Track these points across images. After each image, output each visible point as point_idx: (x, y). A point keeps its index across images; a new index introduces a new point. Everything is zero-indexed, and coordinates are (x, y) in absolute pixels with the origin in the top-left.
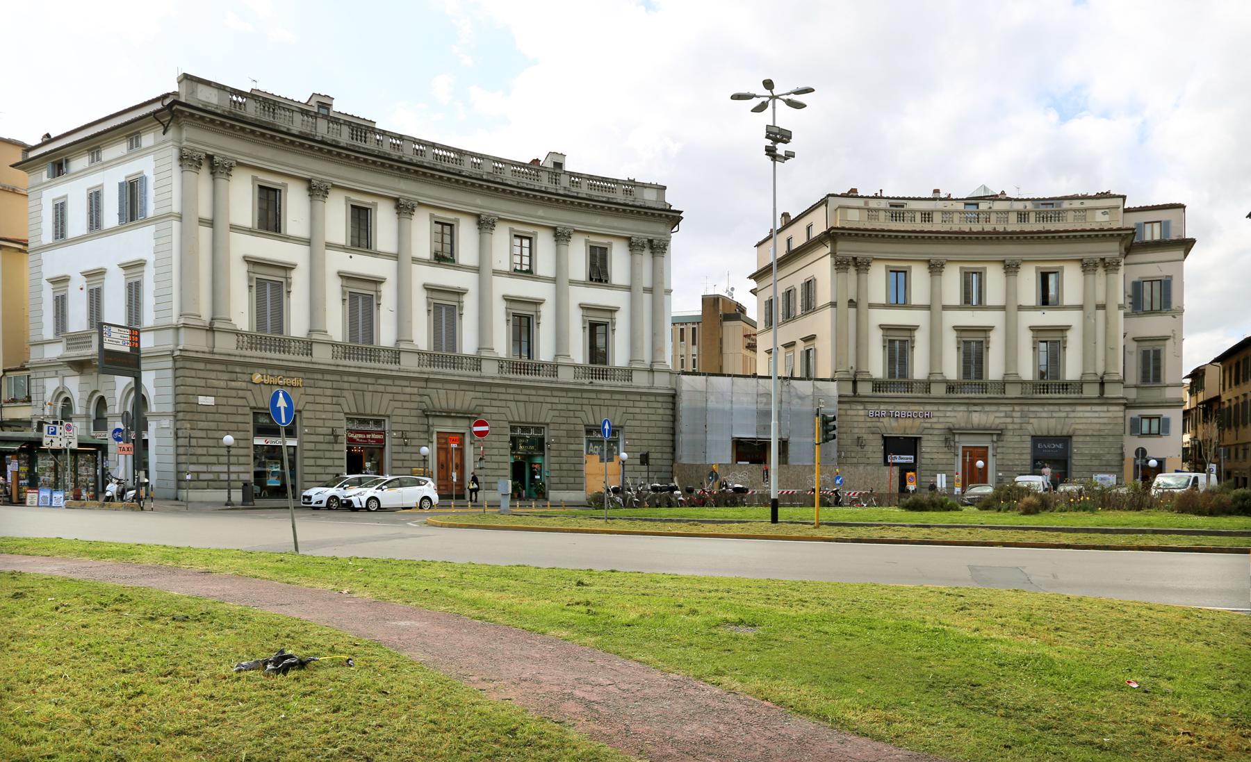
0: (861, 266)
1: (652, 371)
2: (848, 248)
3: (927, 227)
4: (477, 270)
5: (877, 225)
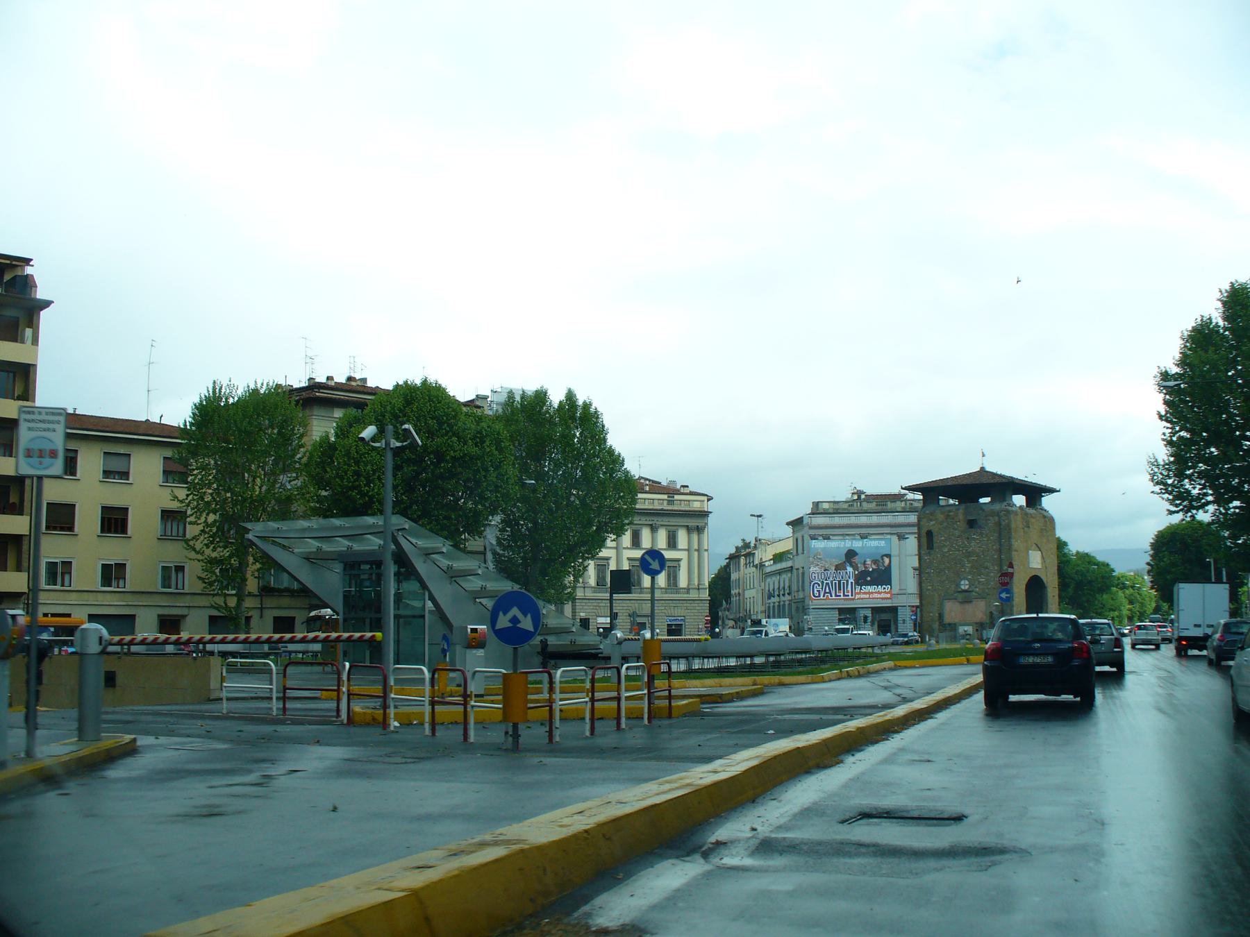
3: (670, 508)
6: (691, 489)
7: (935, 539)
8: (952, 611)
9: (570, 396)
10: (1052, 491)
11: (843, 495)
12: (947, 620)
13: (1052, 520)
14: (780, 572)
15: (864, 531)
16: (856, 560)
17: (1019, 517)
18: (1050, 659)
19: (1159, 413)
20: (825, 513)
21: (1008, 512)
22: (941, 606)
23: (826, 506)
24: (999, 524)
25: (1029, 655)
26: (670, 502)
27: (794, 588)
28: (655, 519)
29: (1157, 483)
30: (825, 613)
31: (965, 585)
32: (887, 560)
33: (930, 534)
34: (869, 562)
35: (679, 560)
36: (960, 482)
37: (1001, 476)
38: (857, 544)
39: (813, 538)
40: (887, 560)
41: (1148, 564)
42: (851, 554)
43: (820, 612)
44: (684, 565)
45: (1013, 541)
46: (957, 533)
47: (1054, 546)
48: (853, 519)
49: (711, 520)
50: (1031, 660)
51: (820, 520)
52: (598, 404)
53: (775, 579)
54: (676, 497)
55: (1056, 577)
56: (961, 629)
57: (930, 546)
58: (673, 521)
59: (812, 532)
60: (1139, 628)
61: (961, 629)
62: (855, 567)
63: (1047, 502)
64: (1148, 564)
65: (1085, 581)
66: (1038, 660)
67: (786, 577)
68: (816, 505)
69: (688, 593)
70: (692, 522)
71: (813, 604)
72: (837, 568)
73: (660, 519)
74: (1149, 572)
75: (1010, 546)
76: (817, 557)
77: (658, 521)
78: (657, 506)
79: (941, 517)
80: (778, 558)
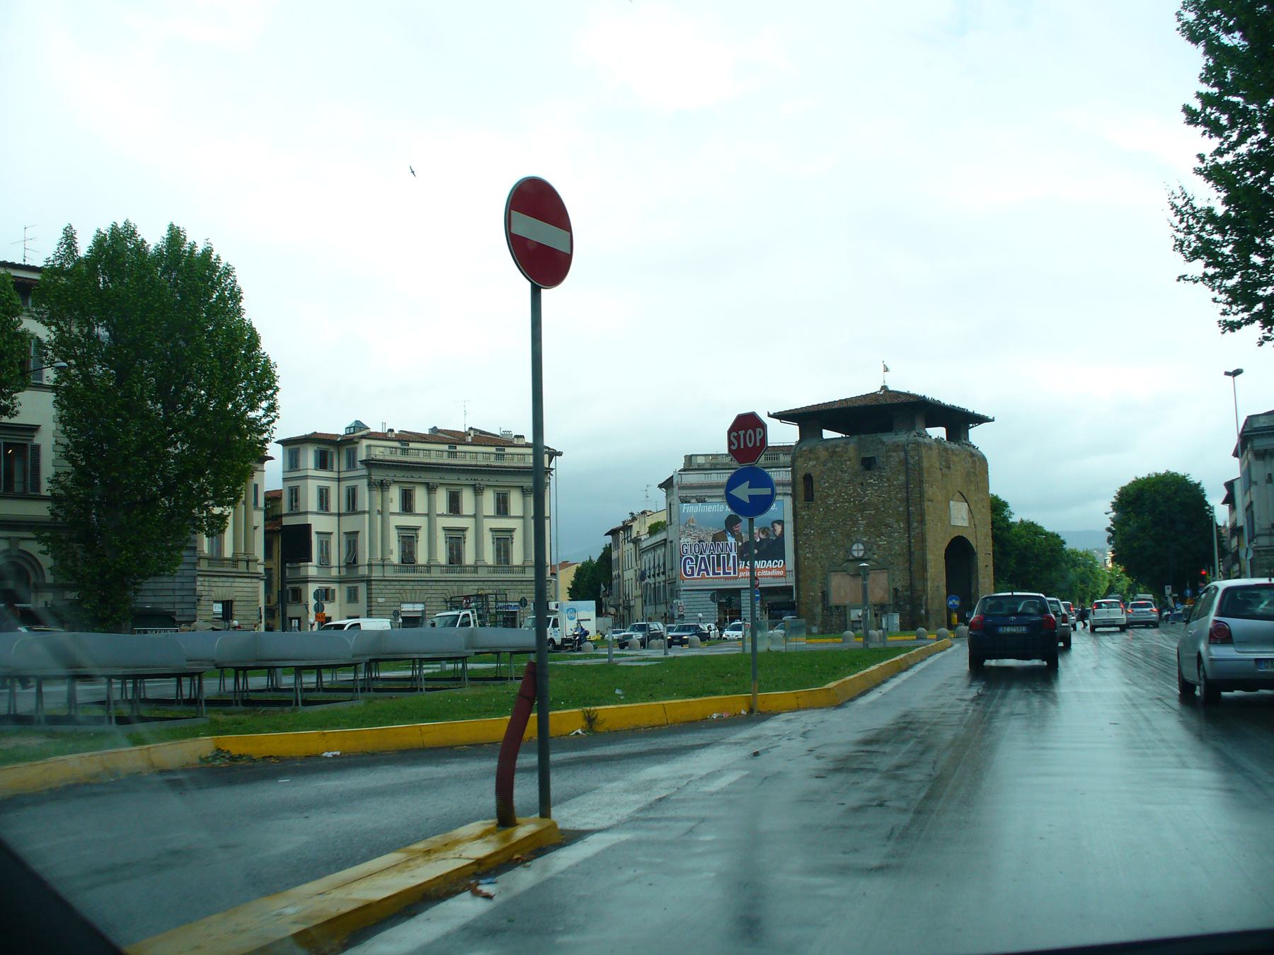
0: (383, 486)
2: (378, 475)
5: (441, 461)
8: (841, 588)
9: (175, 237)
10: (980, 420)
12: (834, 600)
13: (983, 461)
14: (654, 548)
17: (935, 453)
18: (1024, 629)
19: (1187, 109)
20: (700, 468)
21: (918, 444)
22: (825, 583)
23: (701, 460)
26: (500, 456)
27: (668, 566)
28: (479, 477)
29: (1195, 254)
30: (702, 595)
32: (778, 528)
33: (808, 479)
35: (511, 531)
36: (850, 404)
37: (907, 395)
39: (684, 500)
40: (778, 528)
41: (1109, 530)
43: (695, 594)
45: (926, 486)
46: (846, 477)
47: (987, 504)
50: (1008, 630)
52: (225, 254)
53: (650, 555)
54: (508, 450)
55: (990, 541)
57: (809, 496)
59: (684, 493)
62: (738, 537)
63: (976, 435)
64: (1109, 530)
65: (1030, 555)
66: (1014, 630)
67: (660, 552)
68: (689, 459)
69: (476, 572)
71: (683, 585)
72: (716, 538)
73: (485, 477)
74: (1109, 540)
76: (689, 525)
77: (482, 480)
78: (481, 461)
79: (824, 455)
80: (654, 530)
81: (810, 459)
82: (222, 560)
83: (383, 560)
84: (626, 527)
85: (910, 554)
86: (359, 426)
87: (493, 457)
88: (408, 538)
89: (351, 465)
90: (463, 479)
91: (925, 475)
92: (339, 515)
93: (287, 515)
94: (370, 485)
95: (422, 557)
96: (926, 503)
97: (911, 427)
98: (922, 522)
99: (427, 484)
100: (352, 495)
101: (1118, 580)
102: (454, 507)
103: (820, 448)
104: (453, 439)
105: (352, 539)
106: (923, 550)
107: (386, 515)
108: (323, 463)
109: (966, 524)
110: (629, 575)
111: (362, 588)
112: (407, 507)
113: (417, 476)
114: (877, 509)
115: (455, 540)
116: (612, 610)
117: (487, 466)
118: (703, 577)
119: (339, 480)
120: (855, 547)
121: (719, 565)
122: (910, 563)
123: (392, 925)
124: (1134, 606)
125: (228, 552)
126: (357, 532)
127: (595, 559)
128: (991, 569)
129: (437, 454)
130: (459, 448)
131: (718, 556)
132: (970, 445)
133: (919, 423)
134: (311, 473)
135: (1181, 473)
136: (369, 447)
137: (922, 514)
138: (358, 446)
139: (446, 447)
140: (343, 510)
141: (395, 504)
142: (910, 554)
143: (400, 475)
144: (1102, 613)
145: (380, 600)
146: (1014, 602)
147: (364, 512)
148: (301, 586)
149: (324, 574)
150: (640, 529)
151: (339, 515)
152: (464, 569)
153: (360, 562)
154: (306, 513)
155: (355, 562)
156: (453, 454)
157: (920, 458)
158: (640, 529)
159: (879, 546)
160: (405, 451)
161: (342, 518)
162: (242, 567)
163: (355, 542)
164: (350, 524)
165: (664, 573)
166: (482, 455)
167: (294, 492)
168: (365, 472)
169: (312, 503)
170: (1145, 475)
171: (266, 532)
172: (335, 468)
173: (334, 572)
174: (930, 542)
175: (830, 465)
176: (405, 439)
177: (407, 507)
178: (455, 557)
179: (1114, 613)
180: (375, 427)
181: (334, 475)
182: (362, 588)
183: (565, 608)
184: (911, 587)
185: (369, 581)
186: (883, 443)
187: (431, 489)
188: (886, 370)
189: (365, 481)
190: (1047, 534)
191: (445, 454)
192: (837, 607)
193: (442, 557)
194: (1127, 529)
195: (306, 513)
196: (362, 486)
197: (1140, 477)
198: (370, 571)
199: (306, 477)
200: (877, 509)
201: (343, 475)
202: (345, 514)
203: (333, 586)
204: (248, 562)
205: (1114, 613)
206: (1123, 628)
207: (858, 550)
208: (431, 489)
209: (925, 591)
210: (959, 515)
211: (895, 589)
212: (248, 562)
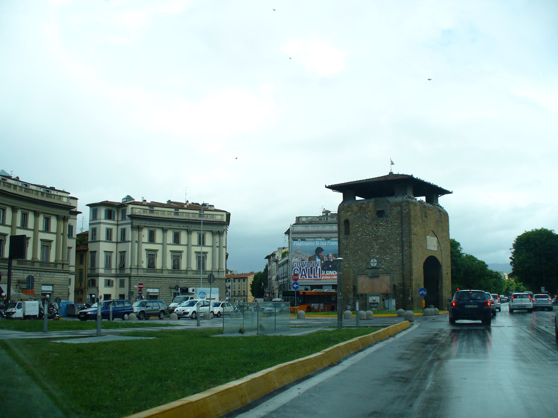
0: (139, 228)
1: (218, 272)
2: (136, 223)
4: (11, 226)
5: (170, 217)
6: (216, 208)
7: (351, 226)
8: (364, 284)
10: (447, 192)
11: (319, 213)
12: (360, 291)
14: (283, 264)
15: (328, 235)
16: (323, 254)
17: (418, 208)
18: (476, 306)
20: (304, 223)
21: (408, 202)
24: (401, 213)
25: (468, 304)
28: (190, 225)
31: (374, 263)
33: (347, 222)
34: (331, 255)
36: (370, 181)
38: (323, 244)
39: (294, 239)
42: (319, 250)
44: (209, 256)
45: (412, 226)
46: (368, 221)
48: (320, 228)
49: (231, 228)
50: (469, 306)
51: (300, 228)
53: (282, 268)
56: (371, 299)
57: (347, 232)
58: (202, 227)
60: (515, 296)
61: (371, 299)
62: (322, 259)
63: (442, 200)
64: (511, 258)
65: (471, 273)
66: (472, 306)
68: (298, 218)
70: (215, 229)
72: (310, 259)
73: (193, 226)
75: (410, 231)
76: (297, 252)
77: (191, 227)
78: (191, 217)
79: (355, 209)
81: (348, 211)
82: (48, 264)
83: (138, 266)
84: (273, 255)
85: (403, 265)
86: (129, 198)
87: (197, 216)
88: (152, 255)
89: (124, 218)
90: (181, 226)
91: (412, 220)
92: (117, 243)
93: (90, 242)
94: (133, 228)
95: (158, 265)
96: (413, 236)
97: (404, 193)
98: (410, 247)
99: (162, 228)
100: (123, 232)
101: (511, 285)
102: (177, 240)
103: (354, 205)
104: (178, 206)
105: (123, 254)
106: (410, 262)
107: (140, 243)
108: (109, 215)
109: (436, 249)
110: (274, 278)
111: (127, 280)
112: (152, 239)
113: (157, 224)
114: (385, 239)
115: (177, 256)
116: (268, 295)
117: (188, 219)
118: (303, 279)
119: (118, 225)
120: (372, 261)
121: (312, 273)
122: (403, 269)
123: (281, 392)
124: (537, 297)
125: (52, 259)
126: (125, 252)
127: (262, 271)
128: (450, 275)
129: (169, 213)
130: (180, 210)
131: (311, 268)
132: (439, 206)
133: (410, 193)
134: (102, 221)
135: (549, 229)
136: (132, 208)
137: (410, 242)
138: (127, 208)
139: (173, 210)
140: (119, 240)
141: (145, 238)
142: (403, 265)
143: (148, 223)
144: (518, 301)
145: (135, 286)
146: (462, 293)
147: (129, 241)
148: (96, 278)
149: (108, 272)
150: (279, 255)
151: (117, 243)
152: (181, 272)
153: (126, 267)
154: (99, 241)
155: (124, 266)
156: (177, 214)
157: (410, 210)
158: (279, 255)
159: (385, 260)
160: (152, 211)
161: (118, 244)
162: (59, 267)
163: (124, 256)
164: (122, 247)
165: (287, 277)
166: (192, 215)
167: (94, 231)
168: (129, 221)
169: (102, 235)
170: (531, 230)
171: (77, 251)
172: (116, 219)
173: (113, 272)
174: (414, 258)
175: (359, 214)
176: (153, 205)
177: (152, 239)
178: (176, 266)
179: (524, 301)
180: (138, 199)
181: (115, 222)
182: (127, 280)
183: (198, 292)
184: (403, 284)
185: (130, 277)
186: (389, 202)
187: (164, 231)
188: (392, 164)
189: (130, 226)
190: (479, 261)
191: (173, 213)
192: (362, 295)
193: (169, 265)
194: (521, 258)
195: (99, 241)
196: (128, 228)
197: (527, 231)
198: (131, 272)
199: (100, 223)
200: (385, 239)
201: (119, 223)
202: (120, 242)
203: (112, 279)
204: (63, 264)
205: (524, 301)
206: (530, 311)
207: (374, 263)
208: (164, 231)
209: (411, 286)
210: (432, 244)
211: (394, 285)
212: (63, 264)
